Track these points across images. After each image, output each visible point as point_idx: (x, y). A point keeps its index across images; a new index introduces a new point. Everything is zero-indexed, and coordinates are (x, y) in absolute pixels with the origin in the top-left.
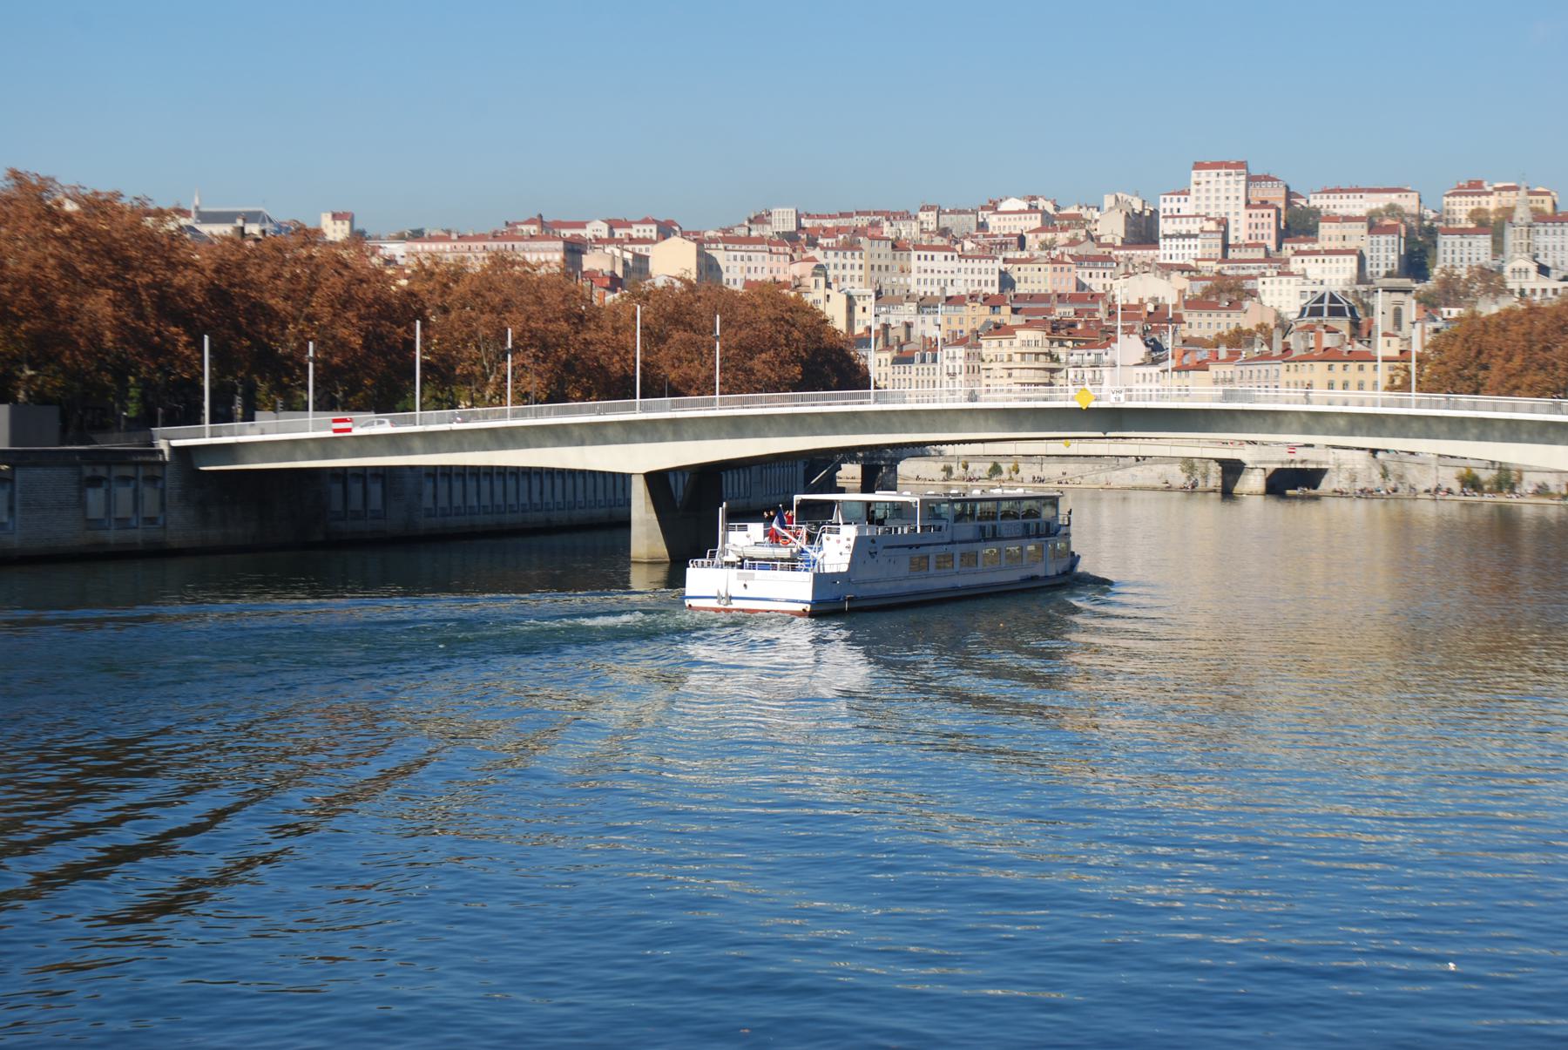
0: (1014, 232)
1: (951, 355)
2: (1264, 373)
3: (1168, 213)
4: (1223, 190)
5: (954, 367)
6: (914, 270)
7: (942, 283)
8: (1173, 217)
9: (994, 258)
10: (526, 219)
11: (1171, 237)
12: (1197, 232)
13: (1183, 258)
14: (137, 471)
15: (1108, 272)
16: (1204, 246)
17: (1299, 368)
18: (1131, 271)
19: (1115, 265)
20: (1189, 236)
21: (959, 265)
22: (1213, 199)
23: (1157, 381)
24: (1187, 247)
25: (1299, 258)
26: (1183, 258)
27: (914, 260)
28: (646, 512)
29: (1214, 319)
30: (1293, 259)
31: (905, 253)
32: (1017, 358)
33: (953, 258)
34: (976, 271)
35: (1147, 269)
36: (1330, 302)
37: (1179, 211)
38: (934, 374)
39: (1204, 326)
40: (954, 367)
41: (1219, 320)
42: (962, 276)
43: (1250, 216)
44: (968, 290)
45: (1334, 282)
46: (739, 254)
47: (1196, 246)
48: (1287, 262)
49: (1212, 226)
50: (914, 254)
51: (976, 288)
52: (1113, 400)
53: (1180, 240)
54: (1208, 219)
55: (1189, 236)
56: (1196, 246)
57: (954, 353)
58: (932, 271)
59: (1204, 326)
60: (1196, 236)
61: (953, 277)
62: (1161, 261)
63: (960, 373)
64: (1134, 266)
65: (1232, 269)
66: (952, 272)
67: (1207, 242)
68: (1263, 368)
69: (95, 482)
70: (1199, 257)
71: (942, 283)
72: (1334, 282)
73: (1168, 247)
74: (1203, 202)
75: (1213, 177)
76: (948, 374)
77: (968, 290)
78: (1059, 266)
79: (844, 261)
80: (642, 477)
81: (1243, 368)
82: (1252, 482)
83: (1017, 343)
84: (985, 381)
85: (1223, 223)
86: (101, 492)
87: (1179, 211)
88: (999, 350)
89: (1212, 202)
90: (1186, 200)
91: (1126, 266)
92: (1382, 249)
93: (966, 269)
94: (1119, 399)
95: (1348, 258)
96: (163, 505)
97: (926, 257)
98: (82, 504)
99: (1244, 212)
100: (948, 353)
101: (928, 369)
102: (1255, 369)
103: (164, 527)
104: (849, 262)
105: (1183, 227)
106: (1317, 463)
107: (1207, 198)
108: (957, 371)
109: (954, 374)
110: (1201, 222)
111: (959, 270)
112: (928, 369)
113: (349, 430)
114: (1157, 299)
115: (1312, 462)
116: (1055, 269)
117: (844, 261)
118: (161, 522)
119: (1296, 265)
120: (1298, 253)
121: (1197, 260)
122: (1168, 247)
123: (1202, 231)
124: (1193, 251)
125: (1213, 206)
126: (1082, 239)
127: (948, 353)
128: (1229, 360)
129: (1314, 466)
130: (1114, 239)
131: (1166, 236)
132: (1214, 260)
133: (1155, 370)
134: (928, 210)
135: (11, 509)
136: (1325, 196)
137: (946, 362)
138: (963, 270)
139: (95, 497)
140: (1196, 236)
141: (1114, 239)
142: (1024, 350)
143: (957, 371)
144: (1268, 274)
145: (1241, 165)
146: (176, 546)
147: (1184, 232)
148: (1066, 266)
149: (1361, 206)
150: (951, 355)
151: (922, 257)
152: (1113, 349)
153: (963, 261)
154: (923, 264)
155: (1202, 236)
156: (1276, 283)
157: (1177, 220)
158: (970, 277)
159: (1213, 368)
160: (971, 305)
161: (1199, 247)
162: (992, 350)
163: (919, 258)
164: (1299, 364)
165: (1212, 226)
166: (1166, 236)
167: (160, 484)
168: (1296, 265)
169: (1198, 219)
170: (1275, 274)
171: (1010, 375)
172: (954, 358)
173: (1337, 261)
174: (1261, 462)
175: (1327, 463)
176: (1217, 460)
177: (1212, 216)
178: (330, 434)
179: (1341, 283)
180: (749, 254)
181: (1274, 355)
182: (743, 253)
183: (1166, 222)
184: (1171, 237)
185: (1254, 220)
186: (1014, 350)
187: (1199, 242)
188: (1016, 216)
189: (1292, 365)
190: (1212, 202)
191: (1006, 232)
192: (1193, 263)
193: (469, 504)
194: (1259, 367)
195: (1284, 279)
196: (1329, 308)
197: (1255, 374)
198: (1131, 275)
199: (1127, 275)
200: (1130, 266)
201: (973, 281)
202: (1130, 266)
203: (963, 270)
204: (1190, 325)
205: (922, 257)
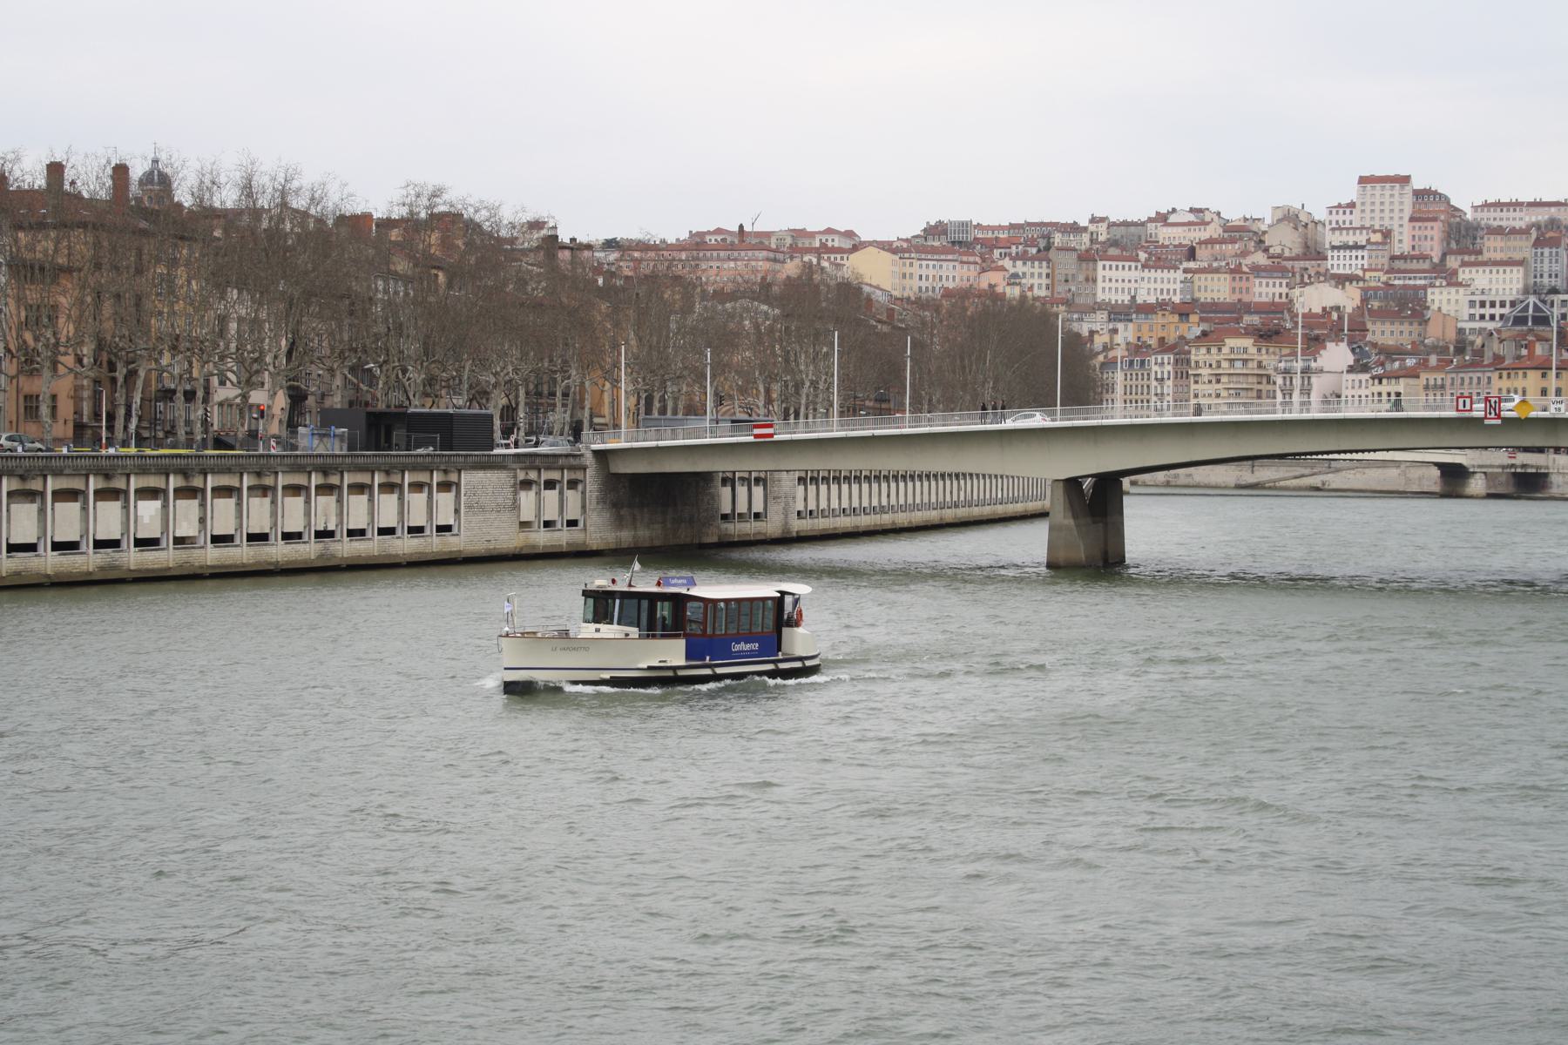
0: (1184, 243)
1: (1159, 361)
2: (1475, 380)
3: (1334, 225)
4: (1387, 204)
5: (1162, 372)
6: (1100, 279)
7: (1133, 292)
8: (1340, 229)
9: (1176, 268)
10: (904, 237)
11: (1338, 248)
12: (1364, 243)
13: (1350, 269)
14: (563, 474)
15: (1284, 282)
16: (1370, 257)
17: (1512, 375)
18: (1307, 281)
19: (1290, 275)
20: (1356, 247)
21: (1142, 275)
22: (1387, 211)
23: (1367, 387)
24: (1354, 258)
25: (1467, 270)
26: (1350, 269)
27: (1103, 271)
28: (1065, 517)
29: (1397, 327)
30: (1461, 270)
31: (1091, 264)
32: (1225, 364)
33: (1136, 268)
34: (1159, 280)
35: (1322, 279)
36: (1534, 311)
37: (1351, 223)
38: (1148, 379)
39: (1387, 333)
40: (1162, 372)
41: (1402, 328)
42: (1145, 285)
43: (1414, 228)
44: (1157, 299)
45: (1507, 292)
46: (931, 263)
47: (1363, 257)
48: (1455, 273)
49: (1377, 237)
50: (1100, 264)
51: (1165, 296)
52: (1553, 411)
53: (1348, 251)
54: (1375, 232)
55: (1356, 247)
56: (1363, 257)
57: (1163, 359)
58: (1123, 281)
59: (1387, 333)
60: (1363, 247)
61: (1137, 285)
62: (1335, 271)
63: (1169, 379)
64: (1310, 277)
65: (1399, 279)
66: (1136, 281)
67: (1374, 254)
68: (1475, 376)
69: (526, 484)
70: (1366, 267)
71: (1133, 292)
72: (1507, 292)
73: (1336, 258)
74: (1368, 215)
75: (1383, 188)
76: (1156, 379)
77: (1157, 299)
78: (1237, 276)
79: (1032, 270)
80: (1061, 484)
81: (1454, 375)
82: (1473, 485)
83: (1225, 350)
84: (1193, 387)
85: (1387, 234)
86: (532, 494)
87: (1351, 223)
88: (1207, 356)
89: (1377, 214)
90: (1351, 213)
91: (1302, 276)
92: (1546, 261)
93: (1174, 283)
94: (1560, 409)
95: (1515, 269)
96: (584, 507)
97: (1117, 267)
98: (515, 506)
99: (1407, 225)
100: (1156, 359)
101: (1137, 374)
102: (1466, 377)
103: (585, 529)
104: (1036, 271)
105: (1350, 239)
106: (1538, 467)
107: (1382, 211)
108: (1166, 376)
109: (1163, 379)
110: (1368, 234)
111: (1143, 279)
112: (1137, 374)
113: (771, 435)
114: (1339, 308)
115: (1532, 467)
116: (1234, 279)
117: (1032, 270)
118: (581, 524)
119: (1464, 275)
120: (1464, 264)
121: (1365, 271)
122: (1336, 258)
123: (1368, 241)
124: (1360, 262)
125: (1377, 219)
126: (1253, 250)
127: (1156, 359)
128: (1437, 369)
129: (1534, 471)
130: (1283, 250)
131: (1333, 248)
132: (1381, 270)
133: (1365, 377)
134: (1098, 222)
135: (457, 511)
136: (1486, 209)
137: (1155, 368)
138: (1146, 280)
139: (527, 499)
140: (1363, 247)
141: (1283, 250)
142: (1232, 357)
143: (1166, 376)
144: (1438, 284)
145: (1406, 180)
146: (595, 548)
147: (1351, 244)
148: (1244, 276)
149: (1521, 219)
150: (1159, 361)
151: (1107, 267)
152: (1321, 355)
153: (1146, 270)
154: (1108, 273)
155: (1368, 247)
156: (1445, 293)
157: (1344, 232)
158: (1152, 286)
159: (1423, 376)
160: (1160, 313)
161: (1366, 257)
162: (1200, 357)
163: (1104, 268)
164: (1512, 373)
165: (1377, 237)
166: (1333, 248)
167: (580, 487)
168: (1464, 275)
169: (1364, 232)
170: (1444, 283)
171: (1218, 381)
172: (1163, 363)
173: (1505, 272)
174: (1480, 466)
175: (1547, 468)
176: (1436, 464)
177: (1377, 227)
178: (751, 439)
179: (1514, 292)
180: (940, 263)
181: (1485, 363)
182: (935, 263)
183: (1333, 234)
184: (1338, 248)
185: (1417, 233)
186: (1222, 357)
187: (1365, 253)
188: (1186, 228)
189: (1505, 373)
190: (1377, 214)
191: (1177, 243)
192: (1360, 273)
193: (832, 507)
194: (1471, 375)
195: (1453, 290)
196: (1533, 317)
197: (1467, 381)
198: (1306, 284)
199: (1303, 284)
200: (1306, 277)
201: (1155, 289)
202: (1306, 277)
203: (1146, 280)
204: (1374, 332)
205: (1107, 267)
